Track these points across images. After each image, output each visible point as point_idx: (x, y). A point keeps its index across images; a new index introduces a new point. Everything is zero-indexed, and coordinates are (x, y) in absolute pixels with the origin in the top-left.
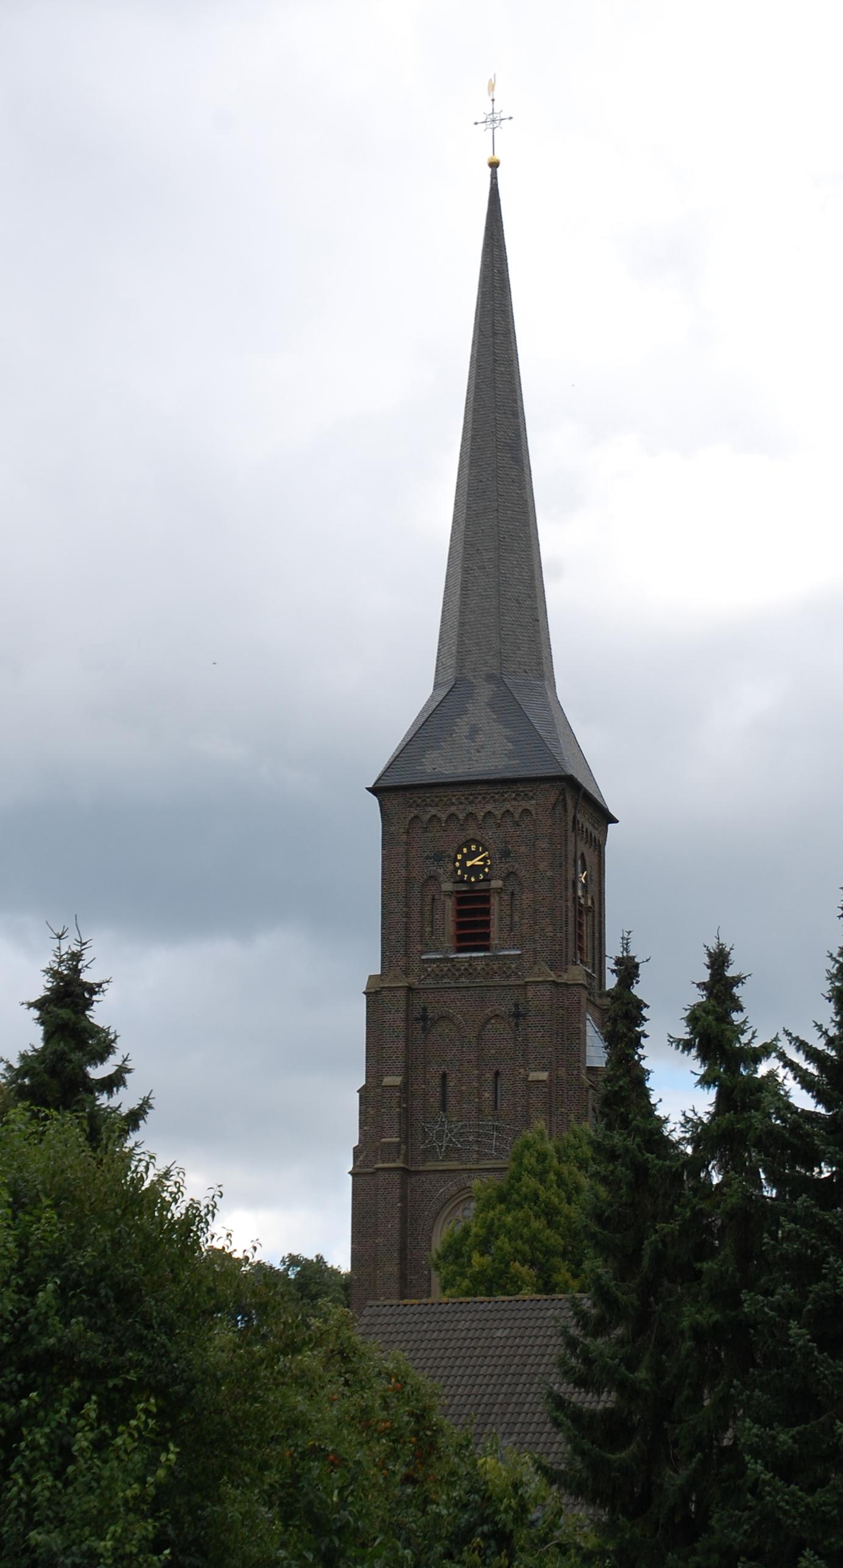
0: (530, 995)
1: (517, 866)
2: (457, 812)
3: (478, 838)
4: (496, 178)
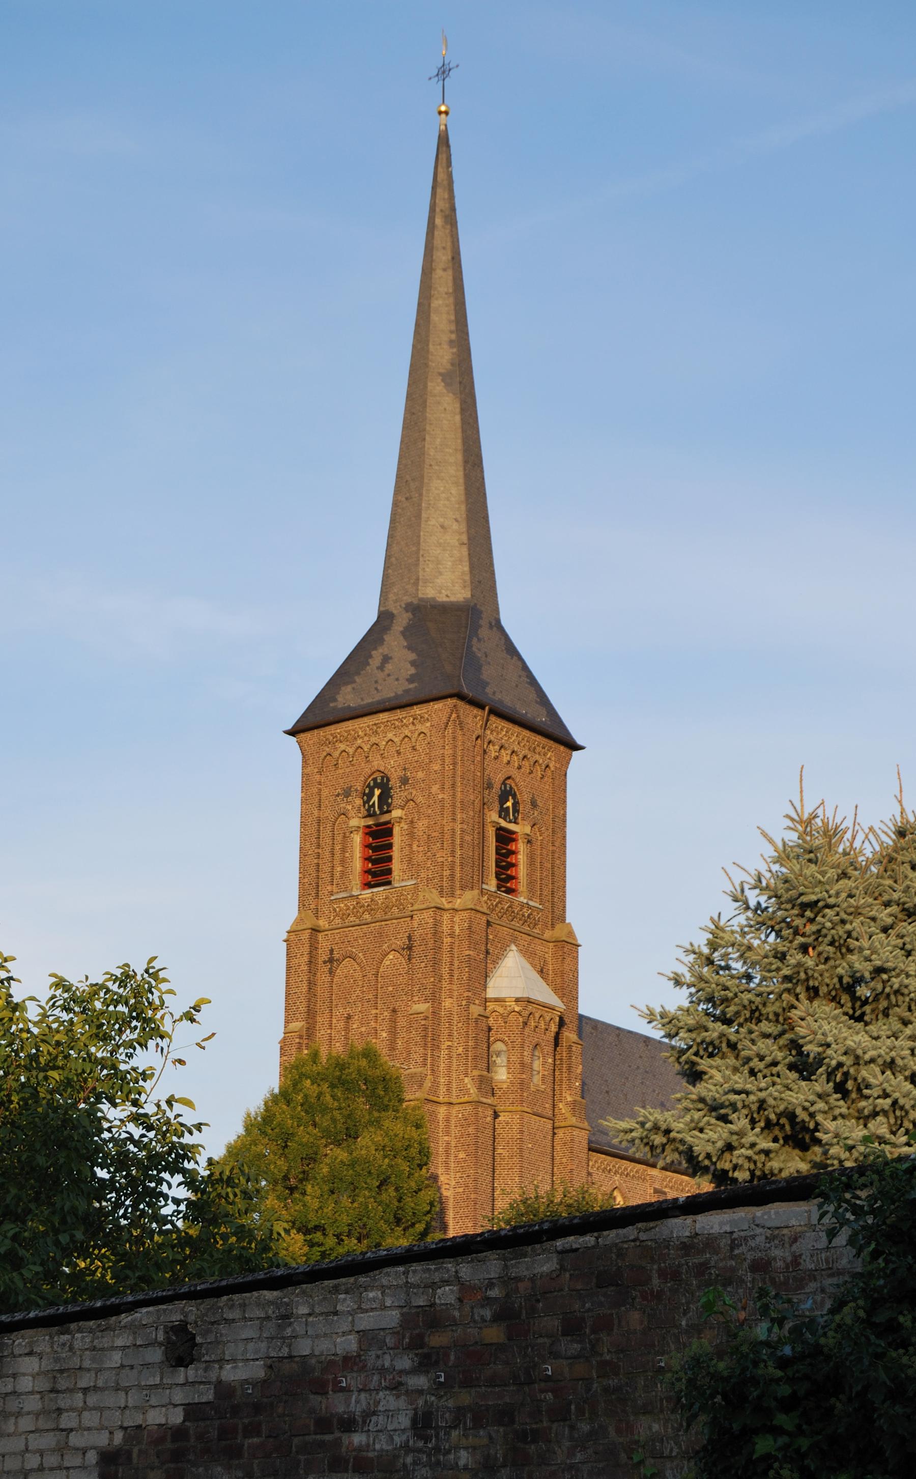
1: (414, 792)
2: (363, 745)
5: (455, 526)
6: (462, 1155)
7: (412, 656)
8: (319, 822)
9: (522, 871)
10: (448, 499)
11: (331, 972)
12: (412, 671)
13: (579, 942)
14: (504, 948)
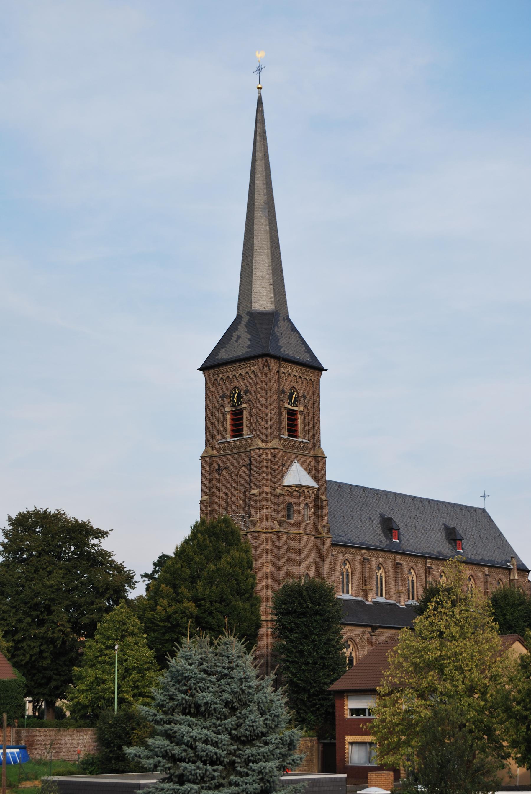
0: (252, 455)
3: (238, 386)
4: (262, 111)
5: (267, 276)
6: (274, 554)
7: (249, 336)
8: (212, 408)
9: (300, 427)
10: (263, 264)
11: (219, 474)
12: (249, 343)
13: (326, 456)
14: (292, 462)
